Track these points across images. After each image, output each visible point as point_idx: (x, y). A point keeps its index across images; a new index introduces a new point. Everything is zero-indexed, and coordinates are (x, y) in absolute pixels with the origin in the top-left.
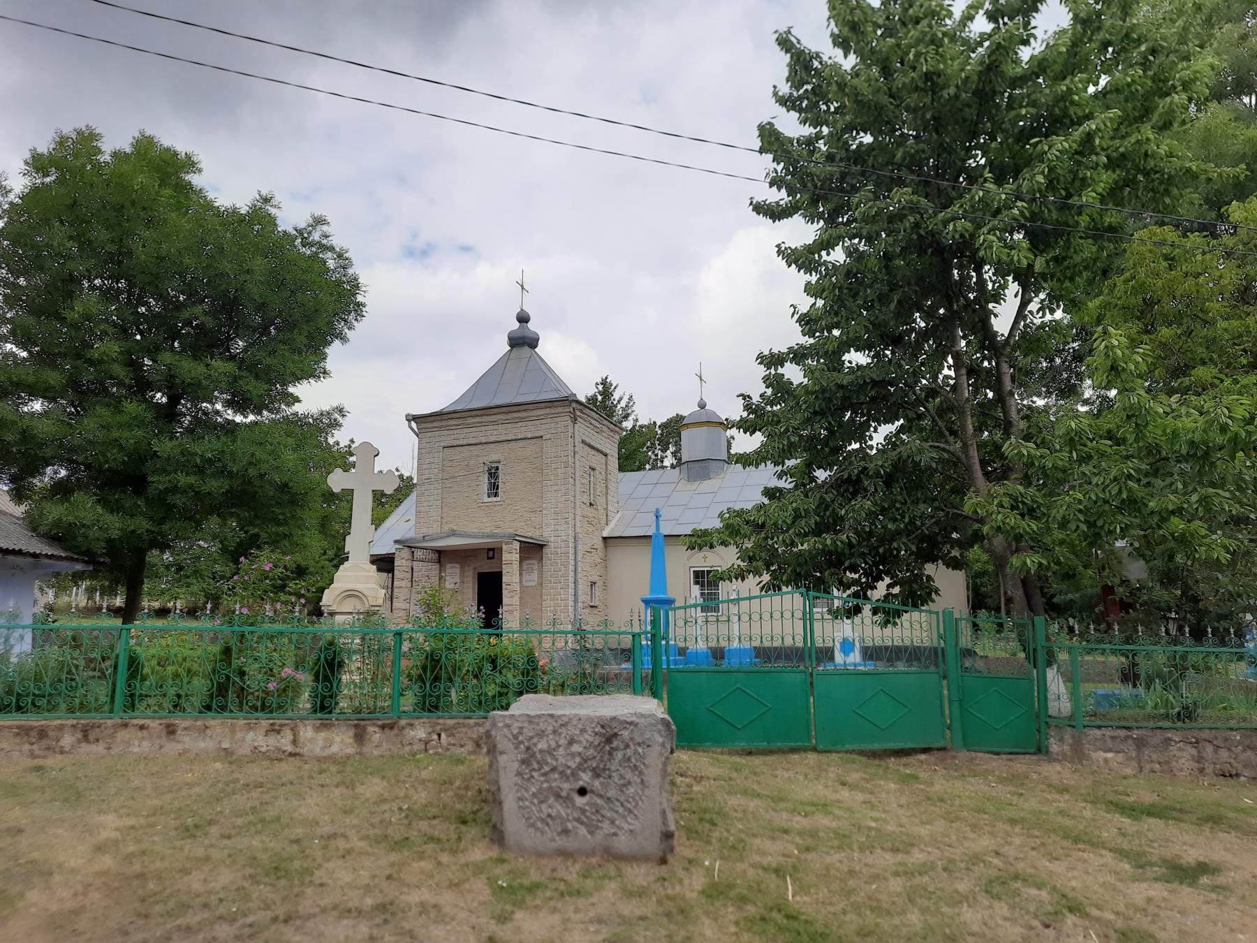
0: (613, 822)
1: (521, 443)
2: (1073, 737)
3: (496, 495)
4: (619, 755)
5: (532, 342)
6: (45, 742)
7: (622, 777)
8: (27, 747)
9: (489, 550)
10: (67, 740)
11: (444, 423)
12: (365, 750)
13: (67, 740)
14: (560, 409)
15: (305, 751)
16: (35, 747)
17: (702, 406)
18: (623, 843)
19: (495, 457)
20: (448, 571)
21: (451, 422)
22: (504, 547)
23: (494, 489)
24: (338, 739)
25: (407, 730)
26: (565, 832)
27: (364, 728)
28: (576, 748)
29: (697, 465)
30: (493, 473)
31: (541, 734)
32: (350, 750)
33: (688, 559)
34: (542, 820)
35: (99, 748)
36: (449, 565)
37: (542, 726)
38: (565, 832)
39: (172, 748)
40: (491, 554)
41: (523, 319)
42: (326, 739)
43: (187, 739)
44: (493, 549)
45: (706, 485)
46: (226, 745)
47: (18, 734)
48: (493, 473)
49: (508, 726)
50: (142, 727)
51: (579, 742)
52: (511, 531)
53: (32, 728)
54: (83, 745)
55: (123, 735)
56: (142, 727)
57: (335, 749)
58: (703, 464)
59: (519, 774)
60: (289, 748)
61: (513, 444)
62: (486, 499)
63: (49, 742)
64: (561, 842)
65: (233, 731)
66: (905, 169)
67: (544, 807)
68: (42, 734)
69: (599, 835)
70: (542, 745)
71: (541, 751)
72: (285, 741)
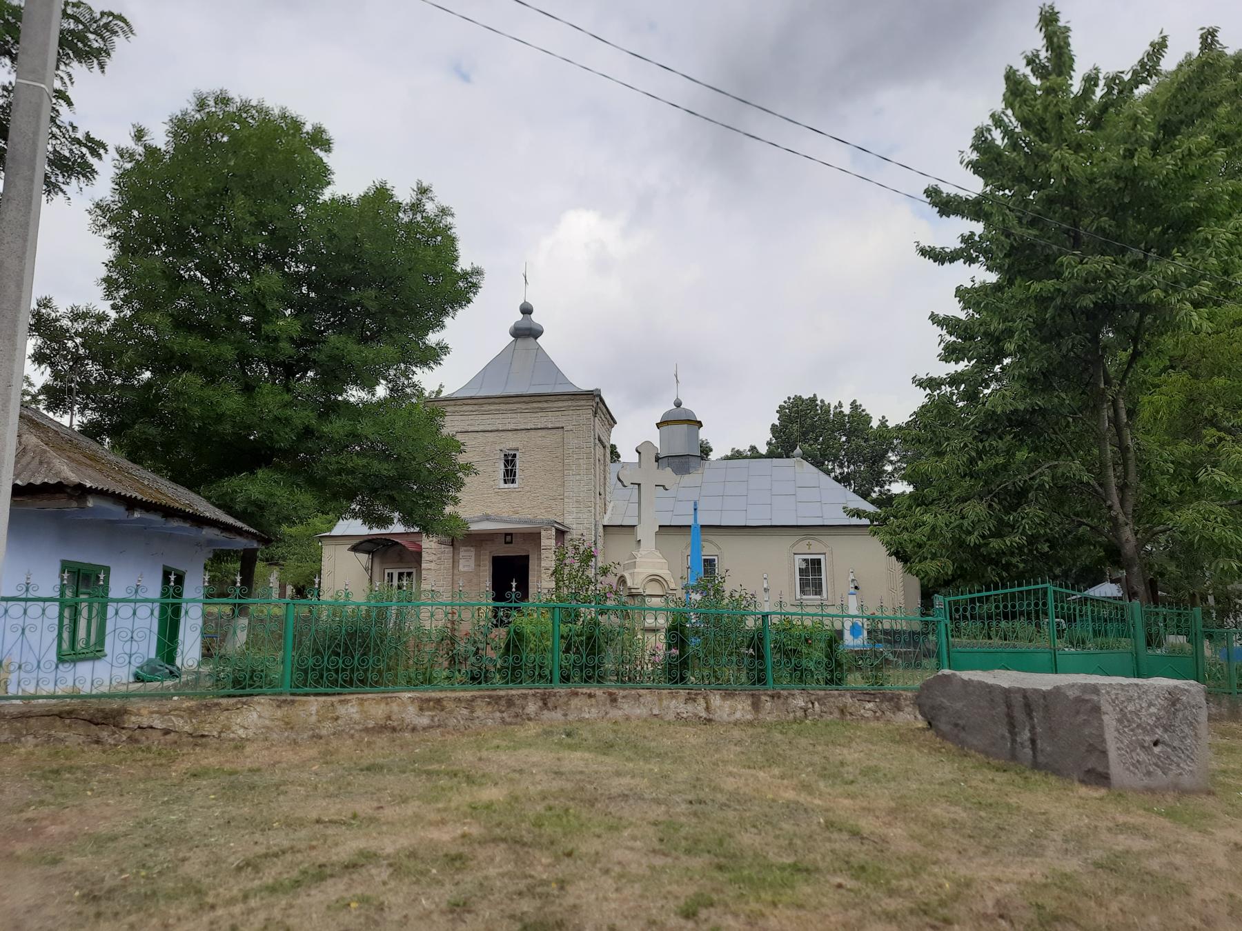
0: (1178, 765)
1: (541, 433)
2: (1230, 702)
3: (513, 481)
4: (1180, 715)
5: (535, 333)
6: (513, 710)
7: (1182, 731)
8: (498, 714)
9: (506, 534)
10: (532, 708)
11: (457, 408)
12: (761, 716)
13: (532, 708)
14: (583, 403)
15: (716, 717)
16: (505, 715)
17: (678, 404)
18: (1186, 781)
19: (513, 445)
20: (462, 554)
21: (465, 408)
22: (543, 533)
23: (510, 475)
24: (740, 707)
25: (790, 700)
26: (1149, 773)
27: (759, 699)
28: (1153, 710)
29: (676, 460)
30: (510, 461)
31: (1130, 699)
32: (749, 717)
33: (794, 545)
34: (1133, 765)
35: (557, 715)
36: (463, 549)
37: (1131, 693)
38: (1149, 773)
39: (616, 714)
40: (509, 538)
41: (526, 310)
42: (730, 707)
43: (626, 706)
44: (511, 534)
45: (687, 479)
46: (656, 712)
47: (489, 703)
48: (510, 461)
49: (1108, 693)
50: (590, 696)
51: (1154, 705)
52: (552, 518)
53: (500, 698)
54: (545, 712)
55: (575, 702)
56: (590, 696)
57: (738, 715)
58: (683, 460)
59: (1117, 730)
60: (704, 714)
61: (532, 432)
62: (502, 485)
63: (517, 710)
64: (1146, 781)
65: (660, 700)
66: (1096, 216)
67: (1134, 755)
68: (510, 702)
69: (1171, 775)
70: (1131, 707)
71: (1131, 712)
72: (700, 709)
